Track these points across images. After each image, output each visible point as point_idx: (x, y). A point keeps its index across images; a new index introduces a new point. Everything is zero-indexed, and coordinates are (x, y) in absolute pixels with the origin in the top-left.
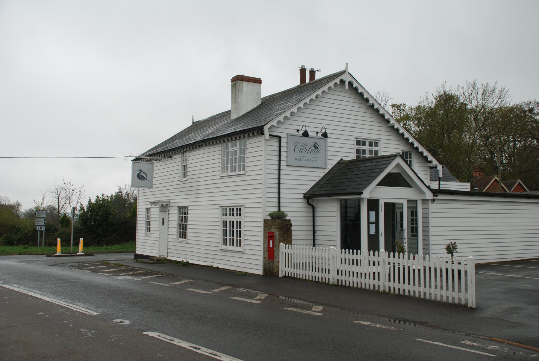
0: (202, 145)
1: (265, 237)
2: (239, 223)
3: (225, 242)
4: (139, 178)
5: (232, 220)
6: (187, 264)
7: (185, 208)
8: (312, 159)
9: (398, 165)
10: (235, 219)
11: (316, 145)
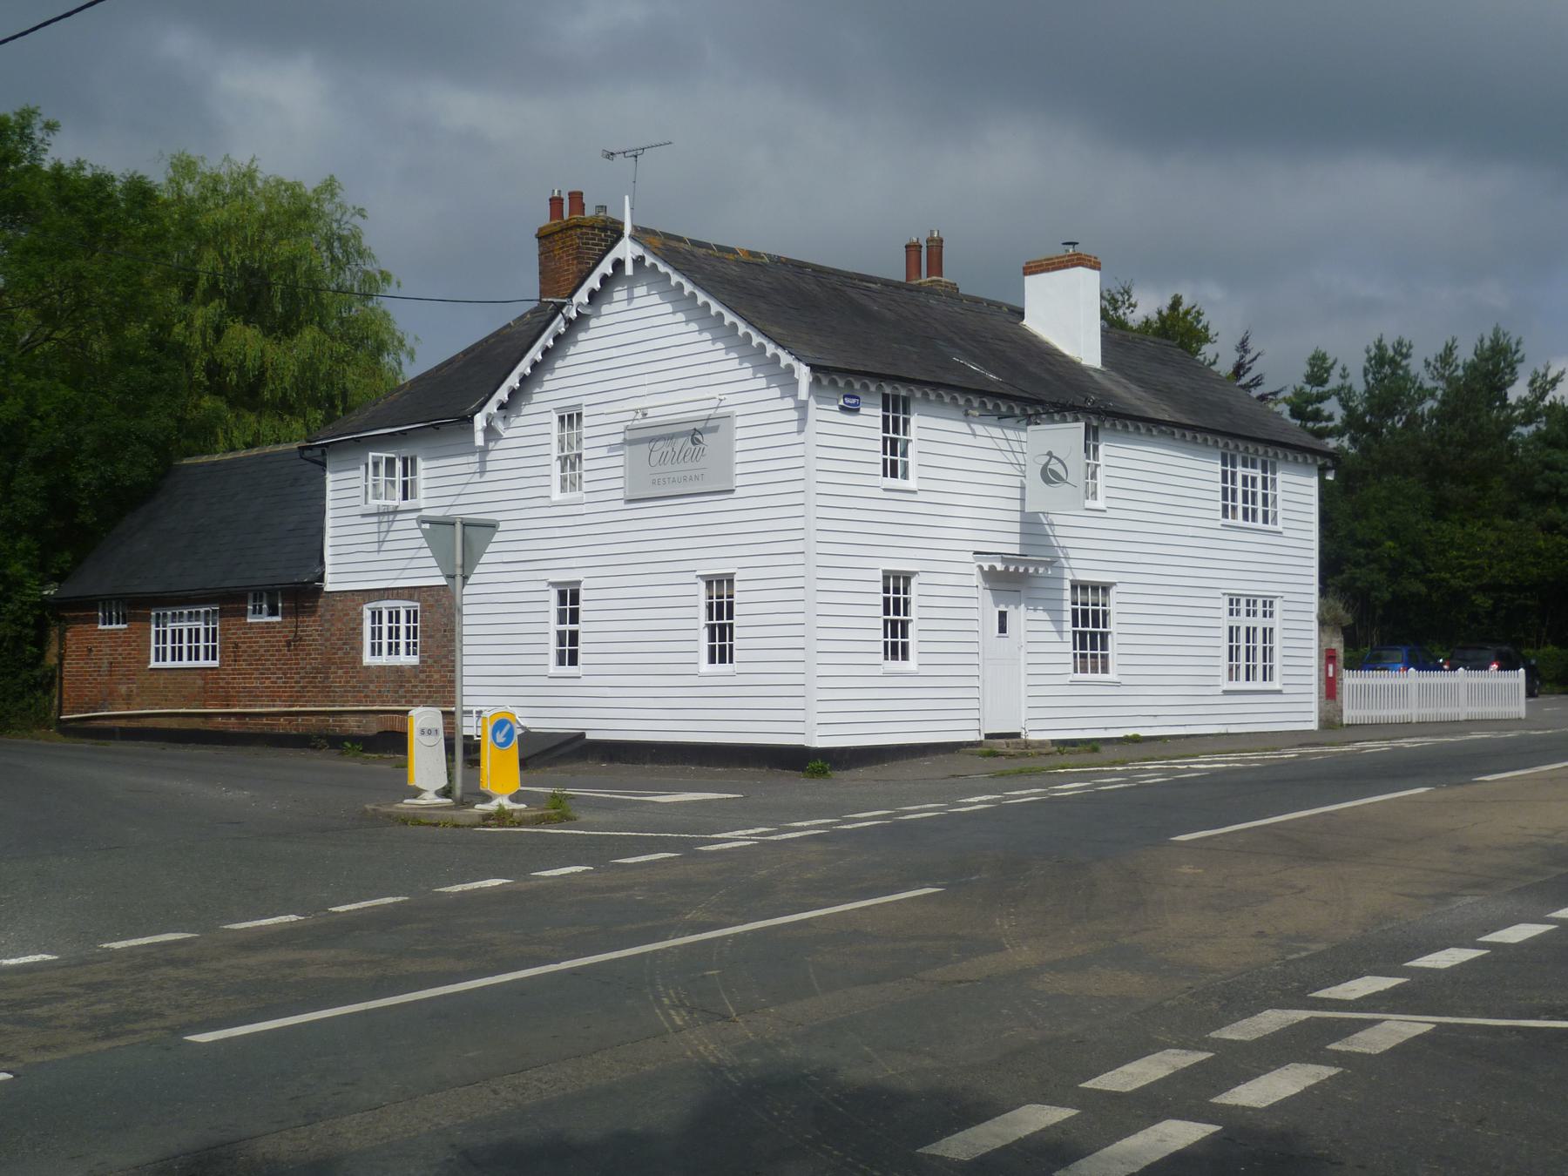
0: (1038, 414)
1: (1320, 657)
2: (1268, 633)
3: (1233, 674)
4: (1047, 481)
5: (1252, 625)
6: (1136, 740)
7: (1095, 588)
8: (688, 474)
9: (376, 650)
10: (1259, 622)
11: (1055, 466)
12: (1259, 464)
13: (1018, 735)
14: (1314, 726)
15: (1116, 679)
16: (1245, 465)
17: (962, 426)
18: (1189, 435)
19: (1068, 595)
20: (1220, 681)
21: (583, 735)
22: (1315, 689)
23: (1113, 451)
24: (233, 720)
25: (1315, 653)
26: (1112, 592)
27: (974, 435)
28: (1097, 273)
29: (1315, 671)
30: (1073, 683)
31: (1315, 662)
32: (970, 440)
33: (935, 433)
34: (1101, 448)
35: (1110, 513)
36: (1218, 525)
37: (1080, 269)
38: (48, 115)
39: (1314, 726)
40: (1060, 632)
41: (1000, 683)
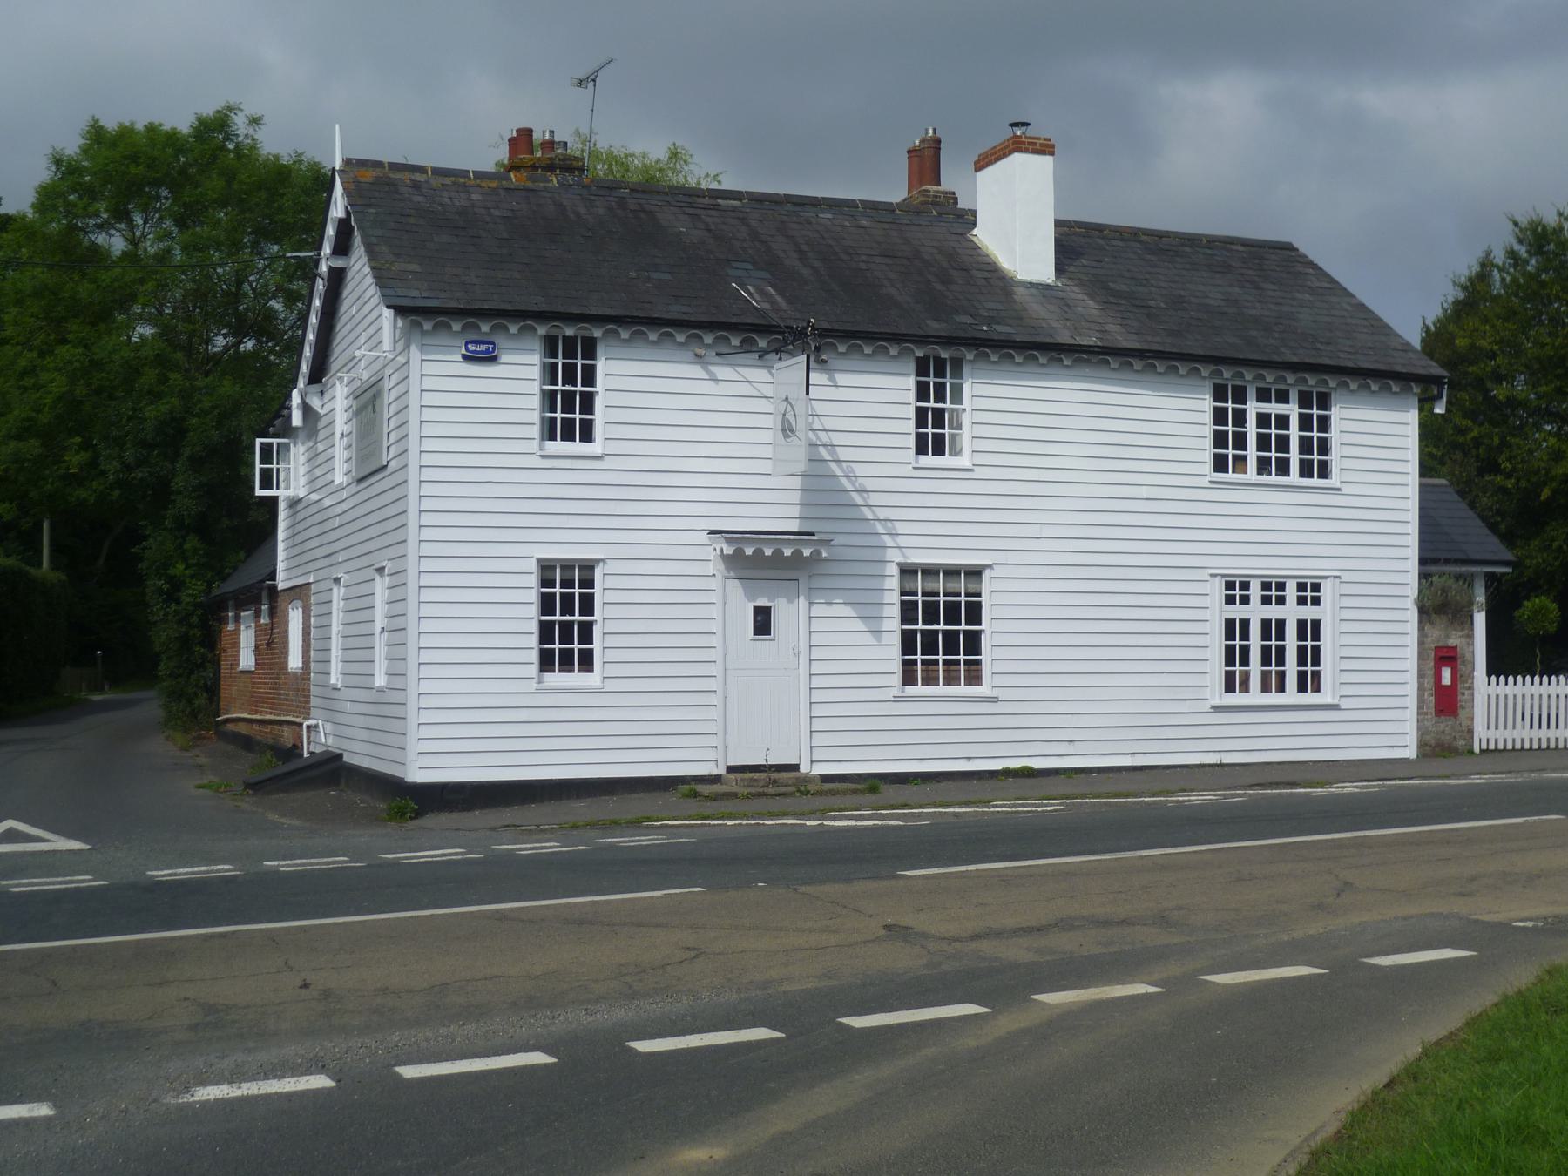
6: (1027, 773)
12: (1294, 396)
13: (795, 767)
14: (1411, 753)
15: (988, 693)
16: (1263, 396)
17: (696, 371)
18: (1138, 364)
19: (893, 583)
20: (1207, 693)
21: (341, 756)
22: (1412, 702)
23: (982, 390)
24: (255, 727)
25: (1412, 652)
26: (986, 575)
27: (716, 380)
28: (1046, 161)
29: (1412, 678)
30: (897, 700)
31: (1412, 664)
32: (709, 387)
33: (628, 380)
34: (967, 387)
35: (978, 473)
36: (1205, 482)
37: (1016, 156)
38: (251, 109)
39: (1411, 753)
40: (877, 632)
41: (828, 700)
